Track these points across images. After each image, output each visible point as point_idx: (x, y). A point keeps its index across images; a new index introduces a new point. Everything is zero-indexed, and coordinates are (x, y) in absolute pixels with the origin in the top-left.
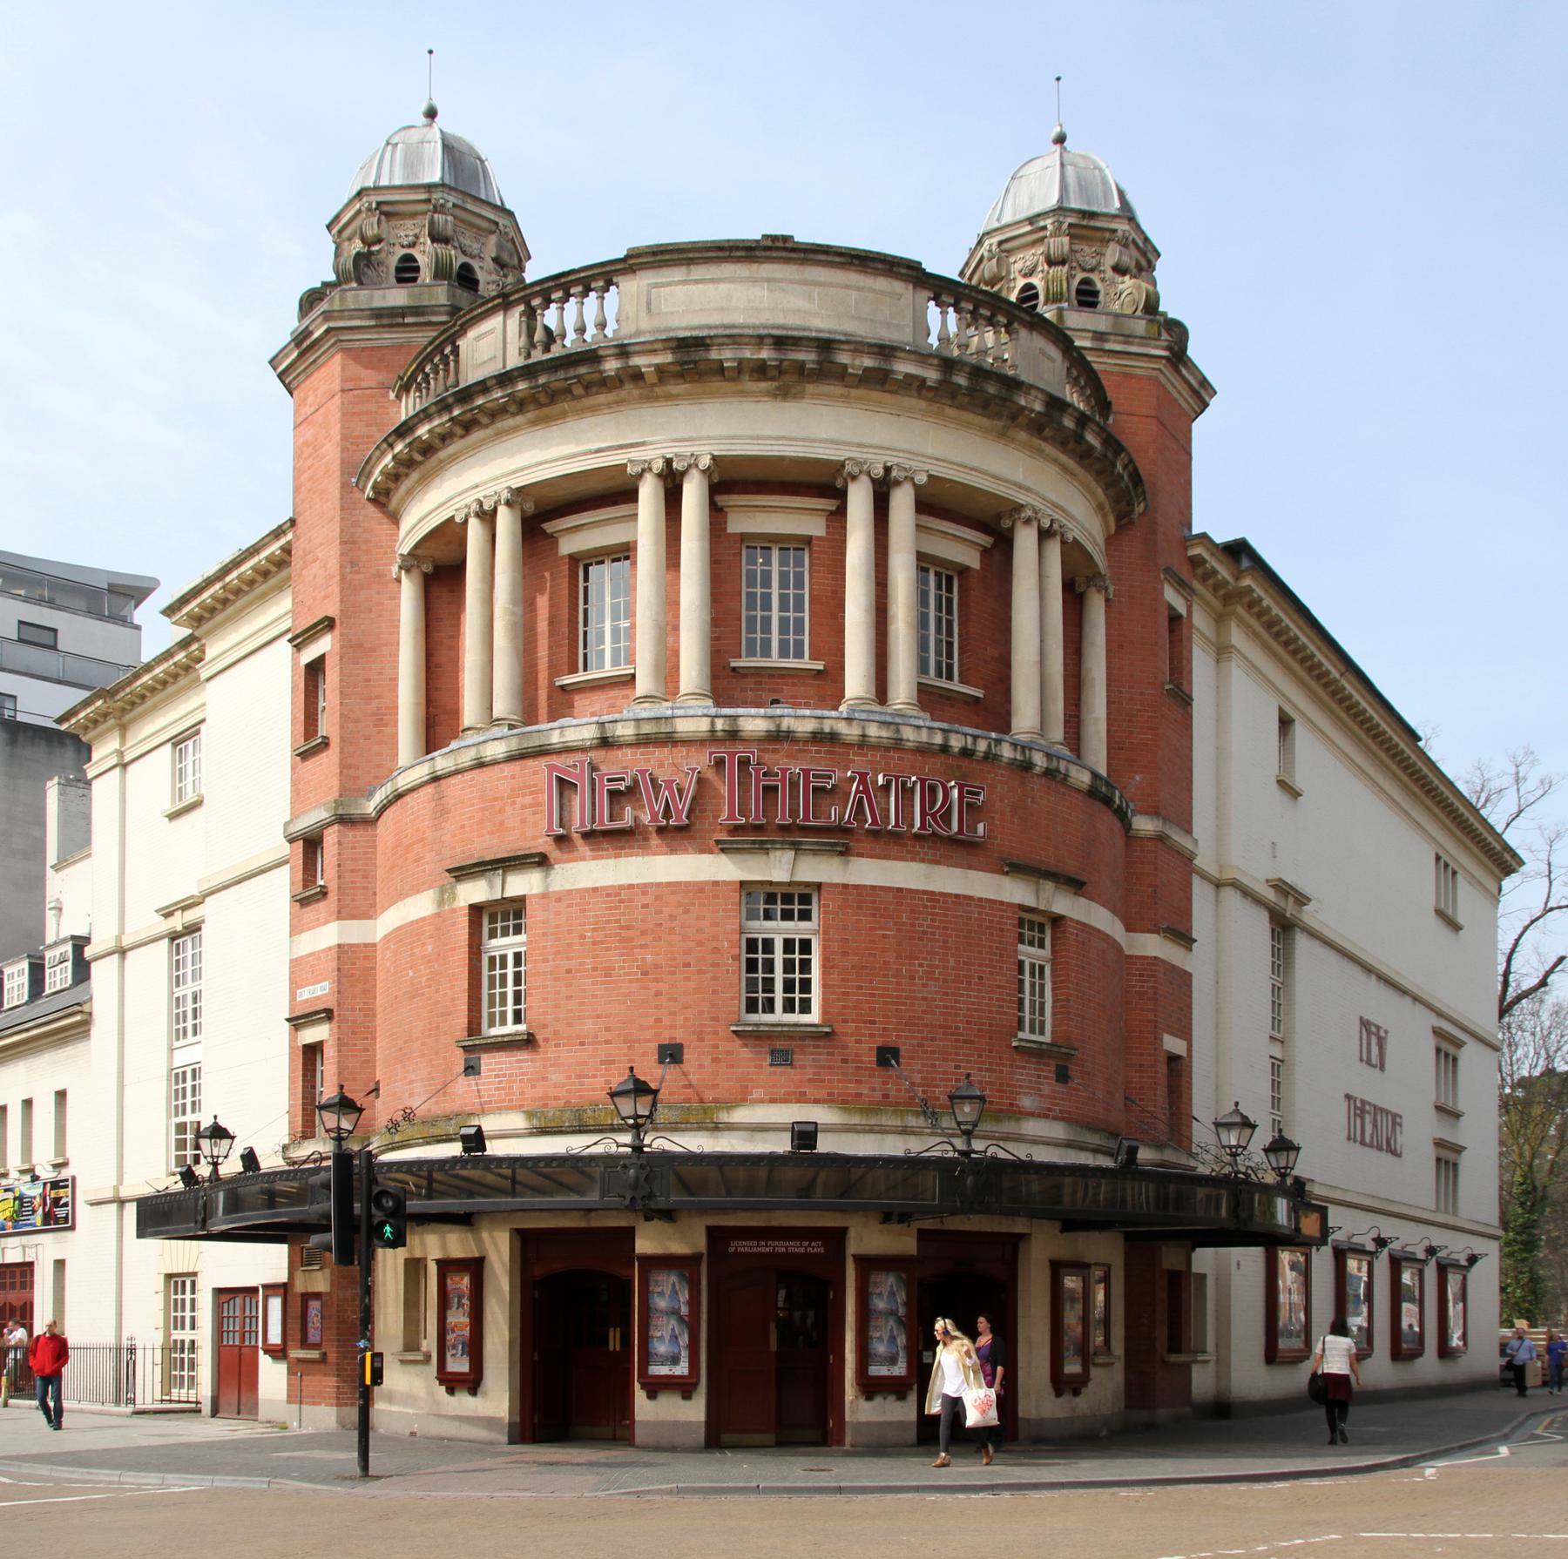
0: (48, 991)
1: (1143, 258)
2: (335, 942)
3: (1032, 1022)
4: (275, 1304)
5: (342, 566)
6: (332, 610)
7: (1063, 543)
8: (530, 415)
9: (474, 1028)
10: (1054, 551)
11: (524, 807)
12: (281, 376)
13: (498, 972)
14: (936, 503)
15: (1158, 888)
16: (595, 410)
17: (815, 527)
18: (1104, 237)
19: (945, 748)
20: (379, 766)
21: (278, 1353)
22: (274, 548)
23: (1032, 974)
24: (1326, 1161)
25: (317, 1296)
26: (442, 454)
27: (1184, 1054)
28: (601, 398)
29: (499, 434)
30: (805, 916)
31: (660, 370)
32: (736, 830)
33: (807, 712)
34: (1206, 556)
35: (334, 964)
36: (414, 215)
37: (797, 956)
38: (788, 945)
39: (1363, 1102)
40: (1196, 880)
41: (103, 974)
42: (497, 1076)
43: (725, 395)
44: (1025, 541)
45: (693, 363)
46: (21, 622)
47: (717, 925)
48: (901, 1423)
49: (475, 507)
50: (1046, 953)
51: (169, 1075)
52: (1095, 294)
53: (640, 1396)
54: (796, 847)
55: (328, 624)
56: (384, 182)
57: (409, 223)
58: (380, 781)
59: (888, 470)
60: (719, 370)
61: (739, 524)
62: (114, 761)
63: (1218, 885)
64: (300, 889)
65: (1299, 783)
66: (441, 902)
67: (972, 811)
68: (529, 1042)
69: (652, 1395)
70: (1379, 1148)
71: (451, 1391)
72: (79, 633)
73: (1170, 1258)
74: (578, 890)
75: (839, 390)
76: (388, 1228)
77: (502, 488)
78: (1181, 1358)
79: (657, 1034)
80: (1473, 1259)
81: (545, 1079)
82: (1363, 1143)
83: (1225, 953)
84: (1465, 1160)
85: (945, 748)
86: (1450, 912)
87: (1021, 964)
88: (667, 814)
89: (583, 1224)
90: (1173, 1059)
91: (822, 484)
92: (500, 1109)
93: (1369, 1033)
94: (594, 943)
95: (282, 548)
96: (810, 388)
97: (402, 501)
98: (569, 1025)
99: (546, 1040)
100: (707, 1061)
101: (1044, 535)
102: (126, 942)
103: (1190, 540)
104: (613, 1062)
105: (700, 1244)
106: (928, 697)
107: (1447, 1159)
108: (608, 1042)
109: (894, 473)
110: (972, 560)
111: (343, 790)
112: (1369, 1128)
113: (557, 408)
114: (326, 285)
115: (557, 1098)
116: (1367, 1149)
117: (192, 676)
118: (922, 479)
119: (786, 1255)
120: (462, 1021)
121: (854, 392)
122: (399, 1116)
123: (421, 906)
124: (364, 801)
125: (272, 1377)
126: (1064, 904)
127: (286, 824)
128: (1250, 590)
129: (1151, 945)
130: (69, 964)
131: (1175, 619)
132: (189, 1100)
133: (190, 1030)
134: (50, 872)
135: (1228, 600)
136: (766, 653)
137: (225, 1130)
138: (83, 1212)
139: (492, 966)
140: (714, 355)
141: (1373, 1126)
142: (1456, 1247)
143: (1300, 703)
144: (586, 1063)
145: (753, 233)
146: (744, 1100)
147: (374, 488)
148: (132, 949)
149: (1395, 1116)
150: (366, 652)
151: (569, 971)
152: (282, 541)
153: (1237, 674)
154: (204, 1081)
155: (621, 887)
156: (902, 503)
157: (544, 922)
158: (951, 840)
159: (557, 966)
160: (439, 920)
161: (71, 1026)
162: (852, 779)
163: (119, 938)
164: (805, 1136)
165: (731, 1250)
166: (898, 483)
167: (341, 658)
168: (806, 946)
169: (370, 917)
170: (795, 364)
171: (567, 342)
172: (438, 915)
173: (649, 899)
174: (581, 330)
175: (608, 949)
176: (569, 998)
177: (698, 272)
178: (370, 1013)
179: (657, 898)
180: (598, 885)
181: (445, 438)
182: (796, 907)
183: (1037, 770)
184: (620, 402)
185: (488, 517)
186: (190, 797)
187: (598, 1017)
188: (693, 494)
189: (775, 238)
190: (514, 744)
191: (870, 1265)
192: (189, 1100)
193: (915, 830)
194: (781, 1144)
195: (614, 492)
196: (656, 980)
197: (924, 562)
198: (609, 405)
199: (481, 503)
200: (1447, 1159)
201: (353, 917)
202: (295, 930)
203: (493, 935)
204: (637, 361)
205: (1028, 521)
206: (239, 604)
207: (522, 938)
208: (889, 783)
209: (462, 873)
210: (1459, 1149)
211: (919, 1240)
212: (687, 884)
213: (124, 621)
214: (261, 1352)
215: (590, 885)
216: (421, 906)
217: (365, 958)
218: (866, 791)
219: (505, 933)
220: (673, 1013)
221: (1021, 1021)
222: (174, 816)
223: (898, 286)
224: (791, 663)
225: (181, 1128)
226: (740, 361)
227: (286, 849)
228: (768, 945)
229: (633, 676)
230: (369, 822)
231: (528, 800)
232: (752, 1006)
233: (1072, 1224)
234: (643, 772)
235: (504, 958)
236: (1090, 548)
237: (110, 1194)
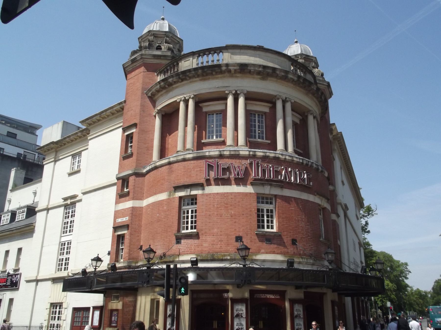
0: (16, 220)
2: (131, 206)
4: (97, 313)
5: (140, 111)
6: (136, 121)
8: (200, 78)
9: (179, 231)
11: (197, 171)
16: (217, 78)
19: (302, 163)
20: (147, 161)
22: (118, 107)
25: (117, 310)
26: (174, 86)
28: (220, 76)
29: (191, 82)
30: (271, 203)
31: (235, 70)
32: (255, 180)
33: (272, 152)
35: (131, 212)
36: (161, 37)
38: (268, 211)
42: (186, 244)
45: (243, 69)
47: (251, 204)
49: (183, 98)
51: (59, 244)
54: (271, 185)
55: (135, 125)
56: (155, 29)
57: (160, 39)
58: (148, 164)
59: (286, 98)
60: (250, 72)
62: (53, 160)
64: (120, 192)
66: (170, 195)
68: (196, 236)
72: (21, 135)
74: (213, 194)
75: (275, 80)
76: (183, 289)
79: (235, 233)
81: (202, 245)
85: (302, 163)
88: (238, 174)
89: (213, 289)
92: (187, 254)
94: (217, 208)
95: (121, 108)
96: (269, 78)
98: (210, 230)
99: (202, 234)
104: (222, 241)
105: (247, 295)
108: (221, 235)
109: (287, 99)
111: (137, 166)
113: (208, 77)
114: (137, 50)
115: (205, 251)
117: (85, 138)
119: (270, 298)
120: (176, 228)
122: (162, 255)
123: (163, 196)
124: (142, 169)
127: (117, 175)
130: (25, 213)
133: (68, 231)
134: (9, 192)
137: (100, 259)
138: (23, 284)
140: (249, 68)
144: (214, 241)
145: (255, 44)
146: (259, 253)
147: (151, 94)
150: (147, 132)
151: (210, 215)
152: (121, 106)
155: (225, 193)
157: (202, 202)
159: (206, 214)
160: (168, 201)
161: (27, 231)
162: (283, 169)
163: (48, 206)
165: (255, 297)
166: (288, 101)
167: (139, 133)
168: (272, 211)
169: (142, 200)
170: (265, 73)
172: (169, 199)
173: (233, 197)
175: (221, 209)
176: (209, 222)
177: (242, 51)
178: (140, 226)
179: (235, 196)
180: (219, 192)
181: (175, 83)
182: (269, 201)
183: (320, 171)
184: (224, 77)
185: (186, 102)
186: (76, 169)
187: (218, 228)
189: (260, 46)
190: (195, 155)
196: (235, 219)
198: (221, 77)
199: (185, 98)
201: (137, 199)
202: (117, 203)
204: (230, 68)
206: (103, 121)
209: (177, 188)
211: (304, 295)
212: (243, 193)
213: (34, 134)
215: (216, 192)
216: (163, 196)
217: (140, 211)
218: (287, 172)
220: (239, 228)
222: (70, 174)
223: (286, 60)
226: (255, 70)
227: (116, 181)
228: (263, 210)
230: (143, 175)
231: (199, 169)
232: (259, 227)
237: (34, 278)
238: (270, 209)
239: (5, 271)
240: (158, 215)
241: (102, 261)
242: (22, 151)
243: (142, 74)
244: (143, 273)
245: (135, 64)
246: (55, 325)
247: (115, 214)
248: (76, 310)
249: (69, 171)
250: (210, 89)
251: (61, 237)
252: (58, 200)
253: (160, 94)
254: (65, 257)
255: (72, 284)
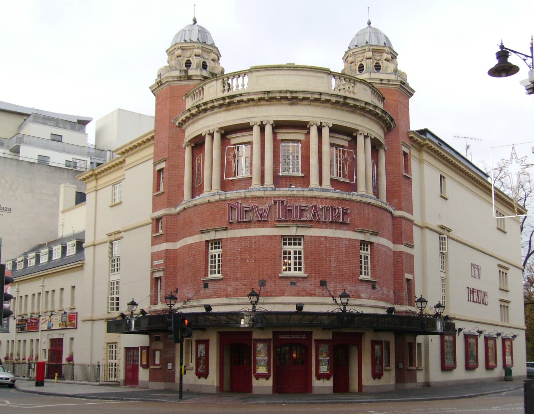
1: (394, 56)
2: (165, 249)
3: (365, 272)
7: (371, 139)
10: (369, 141)
12: (152, 92)
13: (213, 259)
14: (335, 130)
15: (401, 231)
17: (302, 137)
18: (381, 52)
21: (143, 367)
23: (365, 259)
24: (459, 308)
27: (412, 279)
30: (300, 244)
34: (414, 136)
36: (190, 49)
37: (297, 255)
38: (295, 252)
39: (473, 289)
40: (415, 229)
41: (88, 253)
43: (277, 104)
44: (360, 139)
45: (269, 98)
46: (52, 134)
48: (328, 387)
50: (369, 252)
52: (380, 66)
53: (254, 379)
57: (189, 51)
59: (321, 123)
61: (280, 137)
62: (94, 189)
63: (422, 228)
65: (447, 196)
67: (345, 214)
69: (257, 379)
70: (480, 303)
71: (199, 378)
72: (69, 136)
73: (409, 339)
77: (216, 127)
78: (413, 368)
80: (515, 336)
82: (473, 301)
83: (424, 249)
84: (510, 305)
86: (502, 229)
87: (361, 256)
90: (408, 280)
91: (303, 126)
93: (474, 268)
97: (186, 127)
100: (272, 285)
101: (366, 137)
102: (96, 243)
103: (410, 132)
106: (334, 182)
107: (504, 304)
109: (323, 124)
110: (346, 144)
112: (475, 297)
113: (231, 107)
116: (475, 304)
118: (331, 125)
121: (311, 103)
125: (143, 375)
126: (373, 239)
128: (428, 144)
129: (401, 248)
131: (405, 154)
132: (115, 290)
133: (116, 270)
134: (60, 214)
135: (420, 147)
136: (288, 171)
138: (80, 323)
139: (212, 257)
141: (477, 296)
142: (508, 333)
143: (446, 171)
144: (238, 285)
145: (283, 62)
148: (98, 244)
149: (484, 293)
153: (426, 167)
154: (121, 285)
156: (325, 132)
158: (341, 223)
162: (312, 207)
163: (94, 242)
164: (300, 307)
168: (300, 253)
169: (174, 241)
171: (234, 90)
174: (238, 87)
185: (212, 135)
186: (117, 201)
188: (268, 130)
191: (318, 342)
192: (115, 290)
193: (330, 220)
194: (293, 309)
195: (247, 128)
197: (332, 145)
198: (245, 107)
200: (504, 304)
202: (153, 244)
203: (212, 249)
205: (361, 134)
207: (220, 250)
208: (323, 208)
210: (508, 302)
214: (139, 366)
215: (240, 236)
219: (215, 248)
221: (361, 272)
222: (111, 207)
223: (323, 75)
224: (295, 174)
225: (112, 299)
228: (290, 253)
229: (252, 178)
233: (377, 330)
234: (255, 206)
235: (215, 255)
236: (379, 138)
237: (89, 318)
238: (298, 250)
239: (62, 310)
240: (188, 259)
241: (137, 305)
242: (70, 157)
243: (169, 99)
244: (373, 285)
245: (161, 87)
246: (114, 364)
247: (152, 257)
248: (127, 349)
249: (111, 204)
250: (234, 120)
251: (110, 275)
252: (102, 237)
253: (187, 124)
254: (115, 296)
255: (117, 325)
